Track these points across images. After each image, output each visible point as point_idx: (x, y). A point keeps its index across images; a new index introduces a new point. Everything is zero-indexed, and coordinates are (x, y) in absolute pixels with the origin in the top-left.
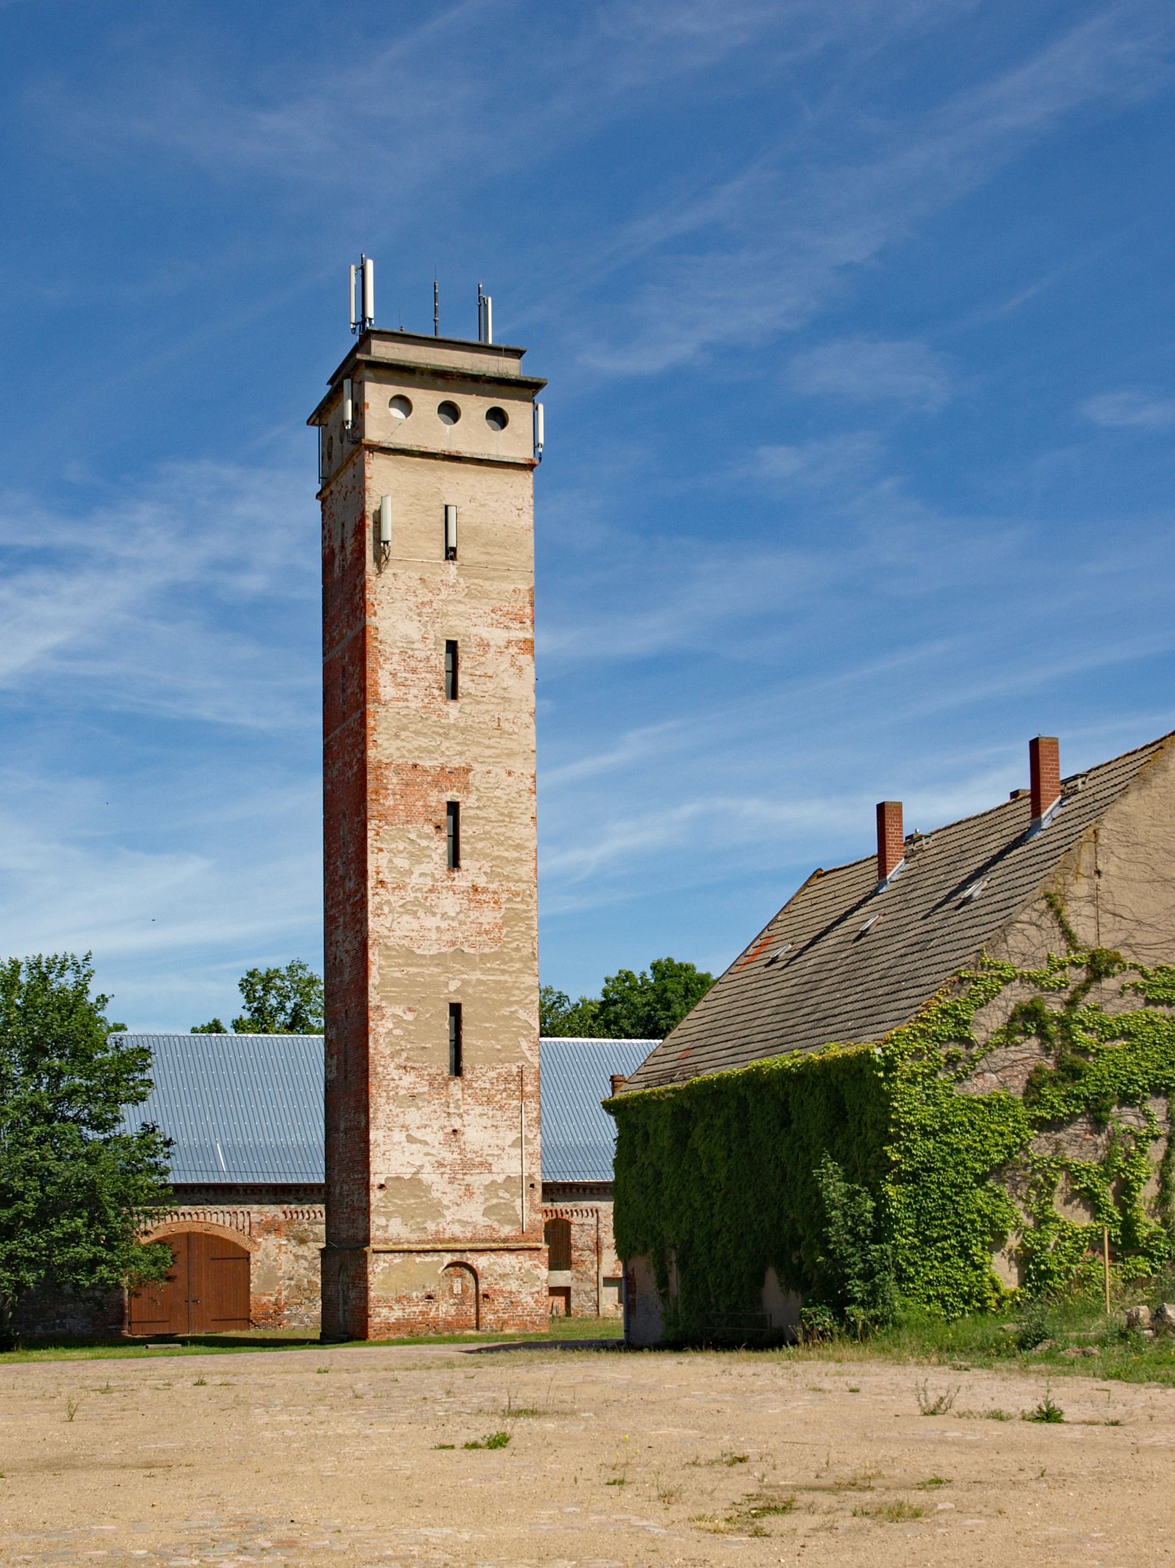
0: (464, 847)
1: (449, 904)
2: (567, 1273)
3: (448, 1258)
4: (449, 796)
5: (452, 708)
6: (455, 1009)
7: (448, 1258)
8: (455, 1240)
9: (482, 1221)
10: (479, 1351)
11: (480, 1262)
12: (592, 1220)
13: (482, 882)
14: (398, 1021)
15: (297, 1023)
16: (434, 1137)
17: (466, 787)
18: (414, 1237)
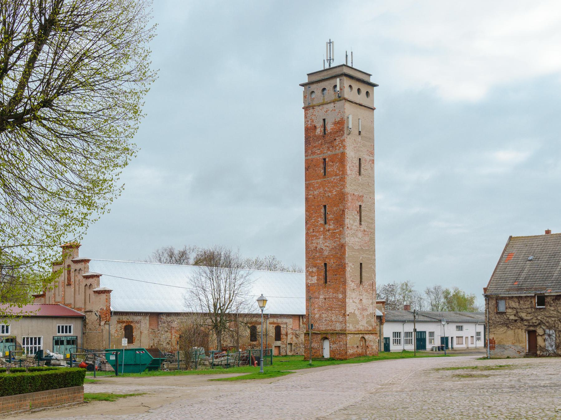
0: (362, 218)
1: (360, 234)
2: (280, 342)
3: (361, 336)
4: (360, 203)
5: (360, 178)
6: (361, 264)
7: (361, 336)
8: (361, 331)
9: (366, 325)
10: (481, 359)
11: (366, 337)
12: (285, 326)
13: (366, 229)
14: (351, 268)
15: (300, 271)
16: (357, 301)
17: (362, 201)
18: (354, 329)
